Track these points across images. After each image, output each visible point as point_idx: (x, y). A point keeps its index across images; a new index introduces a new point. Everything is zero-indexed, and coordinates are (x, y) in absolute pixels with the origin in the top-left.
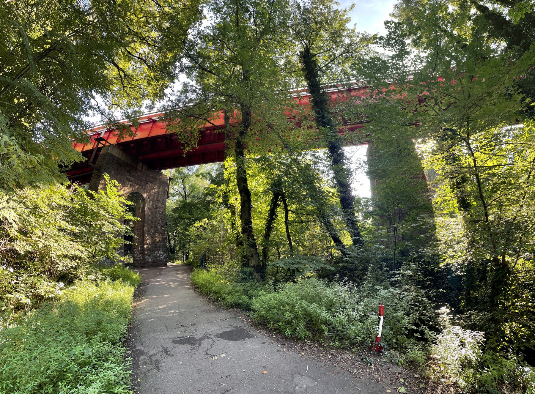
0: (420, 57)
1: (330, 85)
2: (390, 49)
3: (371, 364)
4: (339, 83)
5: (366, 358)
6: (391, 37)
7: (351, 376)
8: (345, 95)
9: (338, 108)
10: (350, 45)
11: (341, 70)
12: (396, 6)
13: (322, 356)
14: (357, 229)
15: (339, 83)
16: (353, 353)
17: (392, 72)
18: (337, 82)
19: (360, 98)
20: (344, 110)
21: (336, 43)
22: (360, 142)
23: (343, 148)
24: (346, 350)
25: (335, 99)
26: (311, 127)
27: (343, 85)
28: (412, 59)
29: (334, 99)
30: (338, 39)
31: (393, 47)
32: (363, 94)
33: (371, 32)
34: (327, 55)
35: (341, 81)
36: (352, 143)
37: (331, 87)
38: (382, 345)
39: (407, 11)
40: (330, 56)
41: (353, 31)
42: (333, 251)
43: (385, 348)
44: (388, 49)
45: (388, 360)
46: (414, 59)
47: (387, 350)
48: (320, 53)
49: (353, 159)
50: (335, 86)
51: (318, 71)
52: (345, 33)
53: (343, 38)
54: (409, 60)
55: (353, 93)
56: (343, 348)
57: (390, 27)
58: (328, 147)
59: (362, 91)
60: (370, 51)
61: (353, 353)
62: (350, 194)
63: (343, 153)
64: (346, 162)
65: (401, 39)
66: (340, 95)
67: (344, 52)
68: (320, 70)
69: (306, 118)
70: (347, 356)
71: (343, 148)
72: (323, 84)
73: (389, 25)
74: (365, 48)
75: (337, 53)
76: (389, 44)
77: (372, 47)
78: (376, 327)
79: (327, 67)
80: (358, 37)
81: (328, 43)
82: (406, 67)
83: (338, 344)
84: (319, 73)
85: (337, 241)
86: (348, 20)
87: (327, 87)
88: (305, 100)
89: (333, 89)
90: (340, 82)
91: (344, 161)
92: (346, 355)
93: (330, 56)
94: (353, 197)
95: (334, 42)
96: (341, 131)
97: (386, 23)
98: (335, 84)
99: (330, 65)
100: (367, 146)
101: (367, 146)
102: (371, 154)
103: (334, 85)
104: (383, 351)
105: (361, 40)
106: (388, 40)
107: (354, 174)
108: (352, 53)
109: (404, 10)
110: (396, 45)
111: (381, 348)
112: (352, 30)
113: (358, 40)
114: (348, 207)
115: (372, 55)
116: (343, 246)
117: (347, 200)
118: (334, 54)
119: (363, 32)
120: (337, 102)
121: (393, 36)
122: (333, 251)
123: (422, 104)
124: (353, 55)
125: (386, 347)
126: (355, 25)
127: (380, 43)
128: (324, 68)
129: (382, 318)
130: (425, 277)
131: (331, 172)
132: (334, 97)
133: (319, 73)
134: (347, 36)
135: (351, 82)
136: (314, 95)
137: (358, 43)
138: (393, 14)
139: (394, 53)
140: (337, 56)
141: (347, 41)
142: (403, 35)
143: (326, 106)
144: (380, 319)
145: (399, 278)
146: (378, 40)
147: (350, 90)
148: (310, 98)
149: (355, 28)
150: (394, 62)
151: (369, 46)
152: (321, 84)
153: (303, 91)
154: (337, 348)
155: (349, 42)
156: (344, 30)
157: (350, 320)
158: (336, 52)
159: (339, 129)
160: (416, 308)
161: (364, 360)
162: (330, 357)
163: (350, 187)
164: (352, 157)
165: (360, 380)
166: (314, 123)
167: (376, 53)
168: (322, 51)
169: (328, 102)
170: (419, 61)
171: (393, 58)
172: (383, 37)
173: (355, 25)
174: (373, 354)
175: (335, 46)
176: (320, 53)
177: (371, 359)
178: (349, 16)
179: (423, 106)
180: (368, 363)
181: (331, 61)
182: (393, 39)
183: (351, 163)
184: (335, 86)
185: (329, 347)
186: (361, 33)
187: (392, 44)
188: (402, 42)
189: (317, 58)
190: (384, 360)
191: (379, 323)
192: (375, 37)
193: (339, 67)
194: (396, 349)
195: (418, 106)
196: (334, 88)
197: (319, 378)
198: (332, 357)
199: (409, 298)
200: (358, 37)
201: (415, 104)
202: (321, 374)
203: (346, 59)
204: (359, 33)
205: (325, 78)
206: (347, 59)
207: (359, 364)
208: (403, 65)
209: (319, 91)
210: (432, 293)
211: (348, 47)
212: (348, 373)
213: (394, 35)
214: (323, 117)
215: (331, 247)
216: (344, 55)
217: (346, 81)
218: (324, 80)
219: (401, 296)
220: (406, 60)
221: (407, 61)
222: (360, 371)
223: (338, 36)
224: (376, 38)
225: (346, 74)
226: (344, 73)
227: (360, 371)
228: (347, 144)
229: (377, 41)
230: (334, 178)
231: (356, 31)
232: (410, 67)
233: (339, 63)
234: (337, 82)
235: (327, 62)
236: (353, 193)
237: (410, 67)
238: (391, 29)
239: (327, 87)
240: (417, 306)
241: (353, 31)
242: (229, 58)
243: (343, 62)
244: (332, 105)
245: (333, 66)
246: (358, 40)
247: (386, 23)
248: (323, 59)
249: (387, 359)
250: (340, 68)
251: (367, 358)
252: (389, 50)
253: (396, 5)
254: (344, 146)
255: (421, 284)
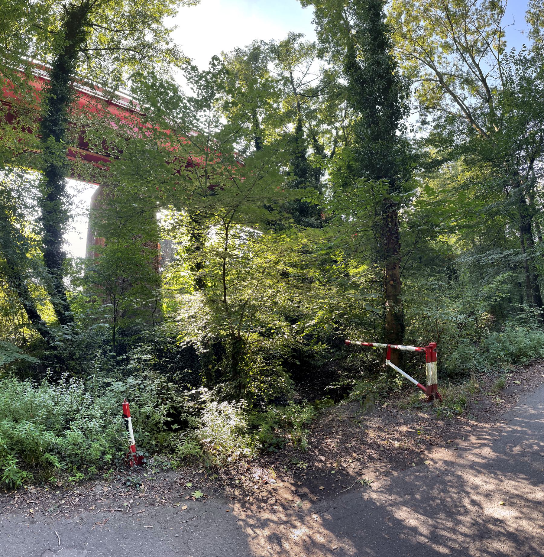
0: (218, 120)
1: (86, 80)
2: (195, 88)
3: (141, 485)
4: (100, 86)
5: (129, 480)
6: (205, 77)
7: (125, 516)
8: (100, 106)
9: (83, 119)
10: (150, 46)
11: (114, 71)
12: (238, 50)
13: (64, 504)
14: (65, 300)
15: (100, 86)
16: (106, 480)
17: (178, 114)
18: (99, 83)
19: (119, 121)
20: (88, 126)
21: (133, 29)
22: (93, 179)
23: (67, 179)
24: (95, 479)
25: (83, 105)
26: (30, 131)
27: (105, 92)
28: (209, 117)
29: (81, 103)
30: (140, 26)
31: (200, 89)
32: (126, 118)
33: (186, 51)
34: (109, 37)
35: (105, 84)
36: (80, 177)
37: (86, 84)
38: (141, 454)
39: (244, 65)
40: (112, 40)
41: (167, 31)
42: (26, 332)
43: (146, 457)
44: (192, 86)
45: (157, 470)
46: (211, 118)
47: (148, 458)
48: (101, 27)
49: (76, 200)
50: (92, 87)
51: (81, 50)
52: (154, 26)
53: (147, 31)
54: (205, 116)
55: (111, 109)
56: (90, 479)
57: (215, 65)
58: (44, 170)
59: (127, 114)
60: (167, 72)
61: (106, 480)
62: (59, 249)
63: (63, 186)
64: (64, 201)
65: (215, 88)
66: (94, 102)
67: (134, 49)
68: (85, 51)
69: (26, 112)
70: (100, 488)
71: (67, 179)
72: (76, 74)
73: (216, 62)
74: (165, 64)
75: (125, 43)
76: (197, 82)
77: (173, 68)
78: (125, 433)
79: (98, 54)
80: (167, 43)
81: (123, 20)
82: (198, 120)
83: (79, 475)
84: (80, 53)
85: (34, 315)
86: (173, 13)
87: (80, 81)
88: (38, 85)
89: (86, 89)
90: (102, 84)
91: (62, 198)
92: (100, 487)
93: (112, 40)
94: (64, 254)
95: (130, 25)
96: (71, 154)
97: (214, 58)
98: (94, 83)
99: (103, 52)
100: (96, 187)
101: (96, 187)
102: (98, 199)
103: (92, 84)
104: (145, 460)
105: (168, 51)
106: (201, 77)
107: (70, 220)
108: (144, 57)
109: (242, 62)
110: (203, 89)
111: (141, 458)
112: (166, 29)
113: (164, 48)
114: (54, 267)
115: (166, 77)
116: (44, 323)
117: (54, 256)
118: (119, 43)
119: (177, 44)
120: (84, 109)
121: (208, 77)
122: (26, 332)
123: (190, 168)
124: (143, 61)
125: (147, 454)
126: (175, 27)
127: (190, 74)
128: (91, 52)
129: (129, 419)
130: (160, 359)
131: (40, 210)
132: (83, 100)
133: (80, 53)
134: (155, 31)
135: (117, 93)
136: (55, 83)
137: (161, 52)
138: (226, 55)
139: (195, 96)
140: (121, 47)
141: (149, 37)
142: (221, 87)
143: (66, 108)
144: (127, 421)
145: (133, 364)
146: (189, 67)
147: (109, 103)
148: (46, 84)
149: (172, 30)
150: (188, 105)
151: (172, 65)
152: (74, 73)
153: (41, 67)
154: (80, 482)
155: (151, 41)
156: (158, 21)
157: (86, 433)
158: (123, 41)
159: (70, 150)
160: (165, 396)
161: (128, 483)
162: (77, 499)
163: (61, 238)
164: (74, 196)
165: (141, 514)
166: (35, 127)
167: (173, 79)
168: (104, 25)
169: (71, 105)
170: (215, 124)
171: (190, 100)
172: (197, 70)
173: (175, 27)
174: (135, 471)
175: (127, 32)
176: (101, 27)
177: (135, 478)
178: (178, 9)
179: (190, 171)
180: (135, 485)
181: (109, 48)
182: (206, 80)
183: (71, 204)
184: (92, 87)
185: (67, 485)
186: (174, 42)
187: (201, 85)
188: (213, 92)
189: (92, 30)
190: (153, 472)
191: (127, 427)
192: (188, 61)
193: (113, 63)
194: (159, 452)
195: (184, 168)
196: (89, 89)
197: (85, 542)
198: (80, 499)
199: (153, 387)
200: (167, 43)
201: (182, 164)
202: (83, 534)
203: (129, 59)
204: (172, 40)
205: (85, 66)
206: (130, 61)
207: (124, 493)
208: (195, 116)
209: (66, 82)
210: (177, 376)
211: (144, 47)
212: (119, 514)
213: (211, 78)
214: (55, 122)
215: (21, 326)
216: (131, 52)
217: (112, 88)
218: (82, 69)
219: (142, 386)
220: (202, 113)
221: (203, 115)
222: (132, 501)
223: (143, 23)
224: (190, 64)
225: (117, 78)
226: (115, 76)
227: (132, 501)
228: (72, 176)
229: (187, 68)
230: (40, 219)
231: (171, 35)
232: (202, 123)
233: (116, 59)
234: (99, 83)
235: (101, 47)
236: (64, 248)
237: (202, 123)
238: (214, 69)
239: (80, 81)
240: (164, 394)
241: (167, 31)
242: (410, 155)
243: (123, 60)
244: (75, 111)
245: (107, 57)
246: (164, 48)
247: (214, 58)
248: (99, 38)
249: (156, 468)
250: (115, 66)
251: (130, 478)
252: (192, 89)
253: (239, 49)
254: (68, 176)
255: (158, 368)
